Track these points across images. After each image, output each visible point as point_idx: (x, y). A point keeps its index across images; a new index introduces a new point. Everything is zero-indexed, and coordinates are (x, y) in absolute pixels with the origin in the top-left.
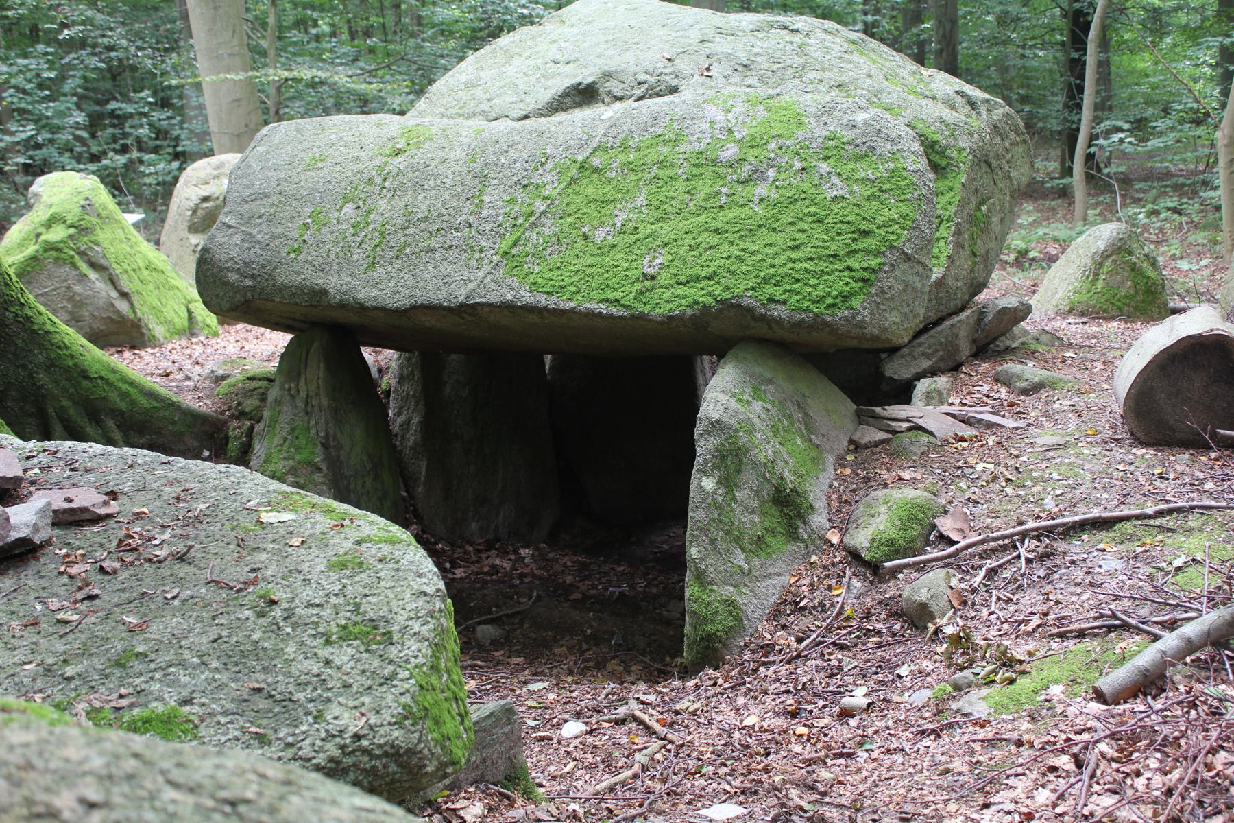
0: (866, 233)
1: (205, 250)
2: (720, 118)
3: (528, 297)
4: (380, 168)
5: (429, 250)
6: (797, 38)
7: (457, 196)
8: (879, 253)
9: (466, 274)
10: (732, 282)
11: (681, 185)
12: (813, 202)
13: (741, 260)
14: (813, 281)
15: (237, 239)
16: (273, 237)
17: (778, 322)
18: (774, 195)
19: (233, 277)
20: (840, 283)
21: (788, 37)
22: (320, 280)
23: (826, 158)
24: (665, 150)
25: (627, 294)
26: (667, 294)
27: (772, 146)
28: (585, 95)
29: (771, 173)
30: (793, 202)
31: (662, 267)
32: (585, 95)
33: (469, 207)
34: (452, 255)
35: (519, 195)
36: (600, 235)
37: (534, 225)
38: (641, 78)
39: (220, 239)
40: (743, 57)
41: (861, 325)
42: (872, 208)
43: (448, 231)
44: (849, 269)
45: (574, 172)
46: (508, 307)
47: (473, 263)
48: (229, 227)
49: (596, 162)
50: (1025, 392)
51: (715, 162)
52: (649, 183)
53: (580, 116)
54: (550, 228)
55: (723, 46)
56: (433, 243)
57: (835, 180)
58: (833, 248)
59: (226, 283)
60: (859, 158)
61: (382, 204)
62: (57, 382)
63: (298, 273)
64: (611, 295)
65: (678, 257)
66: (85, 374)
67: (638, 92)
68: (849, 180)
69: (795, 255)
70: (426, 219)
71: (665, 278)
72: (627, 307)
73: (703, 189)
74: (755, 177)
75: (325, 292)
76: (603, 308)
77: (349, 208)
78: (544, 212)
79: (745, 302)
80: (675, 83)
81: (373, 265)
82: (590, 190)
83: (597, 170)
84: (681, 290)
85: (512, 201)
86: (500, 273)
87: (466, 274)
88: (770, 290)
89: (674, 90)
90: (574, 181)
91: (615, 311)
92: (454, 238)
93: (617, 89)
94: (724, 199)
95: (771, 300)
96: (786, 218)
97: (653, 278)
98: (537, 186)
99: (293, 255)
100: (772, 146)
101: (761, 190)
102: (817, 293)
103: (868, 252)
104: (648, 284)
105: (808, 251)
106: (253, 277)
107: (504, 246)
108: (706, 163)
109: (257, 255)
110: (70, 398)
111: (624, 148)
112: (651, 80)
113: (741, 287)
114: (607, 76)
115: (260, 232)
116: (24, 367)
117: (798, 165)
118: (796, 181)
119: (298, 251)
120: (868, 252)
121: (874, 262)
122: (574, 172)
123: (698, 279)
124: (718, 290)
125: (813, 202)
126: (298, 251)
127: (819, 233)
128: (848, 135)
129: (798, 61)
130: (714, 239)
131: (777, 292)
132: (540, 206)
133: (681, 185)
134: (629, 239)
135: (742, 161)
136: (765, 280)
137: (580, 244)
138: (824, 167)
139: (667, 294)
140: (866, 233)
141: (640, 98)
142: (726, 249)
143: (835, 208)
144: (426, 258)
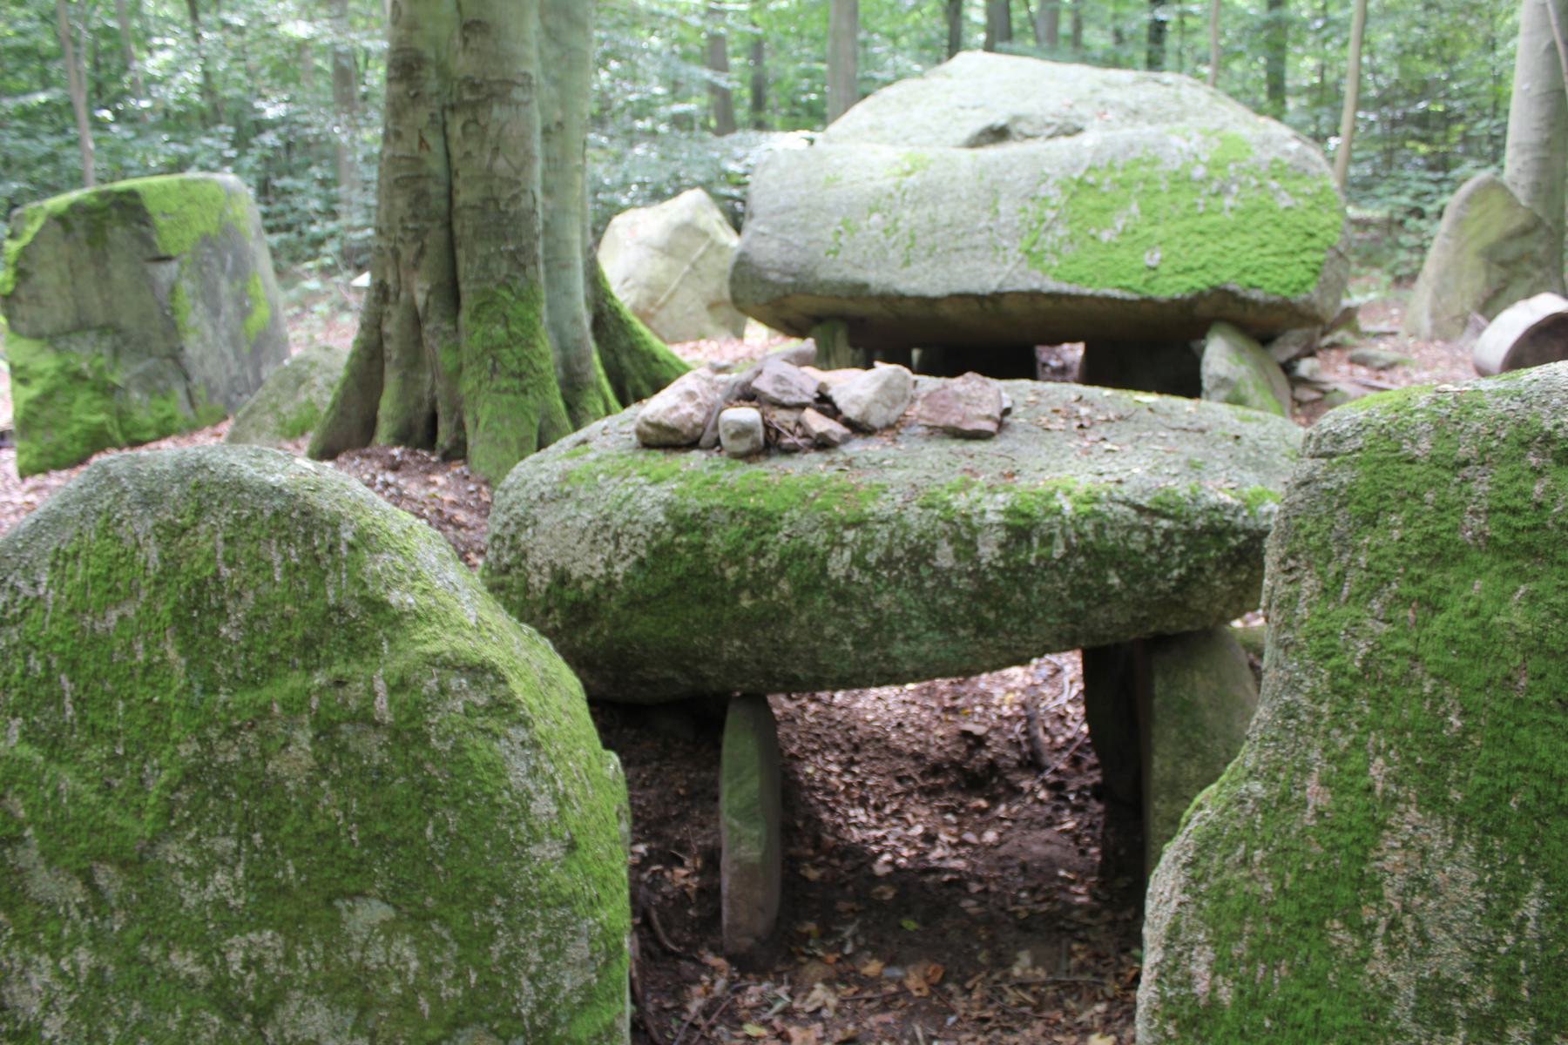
0: (1311, 235)
1: (742, 255)
2: (1184, 145)
3: (1051, 285)
4: (898, 188)
5: (958, 250)
6: (1172, 90)
7: (974, 206)
8: (1322, 251)
9: (994, 268)
10: (1218, 272)
11: (1165, 198)
12: (1271, 211)
13: (1222, 255)
14: (1279, 271)
15: (774, 244)
16: (810, 242)
17: (1255, 303)
18: (1240, 205)
19: (773, 276)
20: (1301, 273)
21: (1163, 90)
22: (860, 276)
23: (1274, 177)
24: (1145, 170)
25: (1136, 281)
26: (1170, 281)
27: (1232, 167)
28: (999, 134)
29: (1235, 188)
30: (1256, 210)
31: (1161, 260)
32: (999, 134)
33: (987, 215)
34: (980, 253)
35: (1030, 206)
36: (1105, 236)
37: (1047, 229)
38: (1050, 119)
39: (757, 244)
40: (1131, 104)
41: (1313, 306)
42: (1313, 215)
43: (972, 234)
44: (1303, 262)
45: (1073, 187)
46: (1034, 295)
47: (999, 259)
48: (763, 234)
49: (1090, 179)
50: (1383, 369)
51: (1189, 179)
52: (1137, 195)
53: (992, 152)
54: (1061, 231)
55: (1113, 96)
56: (960, 243)
57: (1284, 194)
58: (1291, 246)
59: (765, 282)
60: (1298, 177)
61: (907, 214)
62: (634, 364)
63: (839, 270)
64: (1123, 283)
65: (1172, 253)
66: (654, 358)
67: (1049, 131)
68: (1294, 194)
69: (1264, 251)
70: (950, 225)
71: (1165, 269)
72: (1138, 292)
73: (1184, 200)
74: (1222, 191)
75: (865, 286)
76: (1117, 294)
77: (876, 218)
78: (1055, 219)
79: (1231, 287)
80: (1080, 124)
81: (907, 263)
82: (1090, 201)
83: (1092, 186)
84: (1180, 278)
85: (1025, 210)
86: (1024, 267)
87: (994, 268)
88: (1249, 278)
89: (1079, 130)
90: (1074, 195)
91: (1128, 295)
92: (979, 239)
93: (1028, 130)
94: (1201, 209)
95: (1251, 286)
96: (1252, 223)
97: (1154, 269)
98: (1044, 199)
99: (831, 256)
100: (1232, 167)
101: (1228, 201)
102: (1285, 280)
103: (1315, 249)
104: (1153, 273)
105: (1272, 248)
106: (794, 275)
107: (1025, 244)
108: (1181, 181)
109: (796, 257)
110: (644, 378)
111: (1111, 168)
112: (1059, 121)
113: (1227, 277)
114: (1017, 119)
115: (797, 239)
116: (612, 351)
117: (1254, 182)
118: (1255, 194)
119: (836, 252)
120: (1315, 249)
121: (1320, 257)
122: (1073, 187)
123: (1191, 270)
124: (1209, 278)
125: (1271, 211)
126: (836, 252)
127: (1279, 235)
128: (1287, 160)
129: (1177, 108)
130: (1200, 239)
131: (1254, 279)
132: (1050, 214)
133: (1165, 198)
134: (1129, 239)
135: (1210, 179)
136: (1245, 270)
137: (1090, 244)
138: (1274, 184)
139: (1170, 281)
140: (1311, 235)
141: (1051, 137)
142: (1210, 247)
143: (1289, 215)
144: (956, 256)
